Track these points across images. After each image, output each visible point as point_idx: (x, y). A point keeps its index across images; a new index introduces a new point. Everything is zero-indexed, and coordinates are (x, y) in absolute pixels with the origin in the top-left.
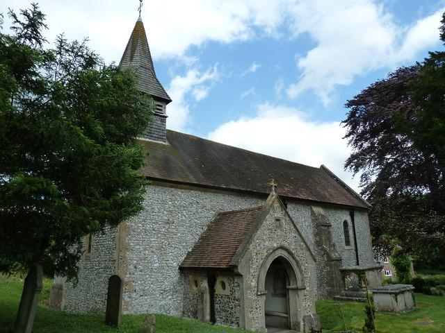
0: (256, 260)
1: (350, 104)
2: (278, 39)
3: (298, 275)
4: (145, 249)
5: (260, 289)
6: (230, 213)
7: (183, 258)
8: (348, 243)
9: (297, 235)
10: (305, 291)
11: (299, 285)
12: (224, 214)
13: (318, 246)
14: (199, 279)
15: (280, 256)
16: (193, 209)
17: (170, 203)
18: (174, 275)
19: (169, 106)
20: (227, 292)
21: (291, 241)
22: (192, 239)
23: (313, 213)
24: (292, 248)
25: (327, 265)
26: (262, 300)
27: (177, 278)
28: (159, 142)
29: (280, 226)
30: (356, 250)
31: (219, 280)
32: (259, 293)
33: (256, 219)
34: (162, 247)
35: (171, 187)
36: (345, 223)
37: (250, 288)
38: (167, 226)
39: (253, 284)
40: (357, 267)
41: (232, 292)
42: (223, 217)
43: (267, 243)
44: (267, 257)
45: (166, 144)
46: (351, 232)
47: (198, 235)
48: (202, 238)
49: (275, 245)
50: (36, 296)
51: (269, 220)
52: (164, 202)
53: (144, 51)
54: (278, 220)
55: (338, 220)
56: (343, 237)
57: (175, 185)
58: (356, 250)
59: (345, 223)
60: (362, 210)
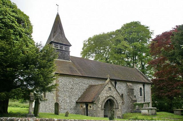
1: (157, 36)
2: (72, 54)
4: (64, 97)
5: (102, 108)
6: (94, 85)
8: (141, 95)
11: (117, 107)
12: (92, 86)
13: (128, 96)
14: (83, 105)
16: (81, 84)
19: (70, 48)
20: (92, 109)
21: (114, 94)
22: (80, 94)
23: (127, 85)
25: (131, 102)
26: (103, 111)
28: (66, 61)
29: (111, 90)
30: (144, 98)
31: (89, 105)
33: (103, 87)
35: (72, 77)
36: (141, 88)
37: (99, 107)
38: (71, 90)
40: (144, 102)
41: (93, 109)
42: (91, 87)
43: (105, 95)
44: (105, 99)
45: (70, 61)
46: (143, 92)
48: (84, 93)
49: (108, 95)
50: (39, 105)
51: (106, 88)
52: (70, 82)
53: (61, 30)
54: (110, 88)
55: (137, 88)
56: (139, 93)
58: (144, 98)
59: (141, 88)
60: (148, 84)
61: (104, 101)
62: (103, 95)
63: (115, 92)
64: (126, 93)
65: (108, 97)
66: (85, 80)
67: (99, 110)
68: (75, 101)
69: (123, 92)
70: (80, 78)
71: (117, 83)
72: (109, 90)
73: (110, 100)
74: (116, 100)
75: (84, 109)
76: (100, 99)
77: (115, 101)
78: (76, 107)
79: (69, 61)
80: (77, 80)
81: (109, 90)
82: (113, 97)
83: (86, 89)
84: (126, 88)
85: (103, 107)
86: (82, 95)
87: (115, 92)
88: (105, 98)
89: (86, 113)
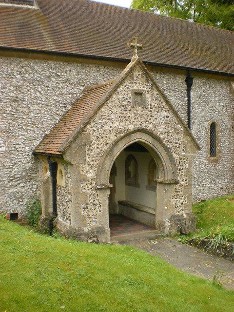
0: (96, 146)
3: (168, 166)
7: (38, 142)
9: (171, 115)
10: (177, 187)
11: (169, 177)
15: (139, 141)
17: (18, 76)
18: (25, 161)
22: (49, 122)
24: (160, 131)
27: (30, 164)
29: (143, 104)
32: (98, 187)
34: (9, 129)
37: (84, 180)
38: (16, 105)
39: (89, 175)
43: (116, 124)
44: (116, 143)
45: (35, 7)
47: (58, 115)
49: (131, 127)
51: (124, 93)
54: (138, 94)
57: (23, 54)
61: (110, 152)
62: (106, 127)
63: (164, 114)
64: (226, 120)
65: (129, 134)
66: (68, 68)
67: (87, 189)
68: (27, 149)
69: (216, 117)
70: (50, 62)
71: (196, 82)
72: (136, 103)
73: (136, 149)
74: (167, 150)
75: (46, 182)
76: (88, 143)
77: (163, 154)
78: (31, 169)
79: (30, 7)
80: (38, 69)
81: (136, 103)
82: (150, 133)
83: (73, 104)
84: (228, 100)
85: (105, 180)
86: (55, 125)
87: (164, 114)
88: (113, 138)
89: (51, 196)
